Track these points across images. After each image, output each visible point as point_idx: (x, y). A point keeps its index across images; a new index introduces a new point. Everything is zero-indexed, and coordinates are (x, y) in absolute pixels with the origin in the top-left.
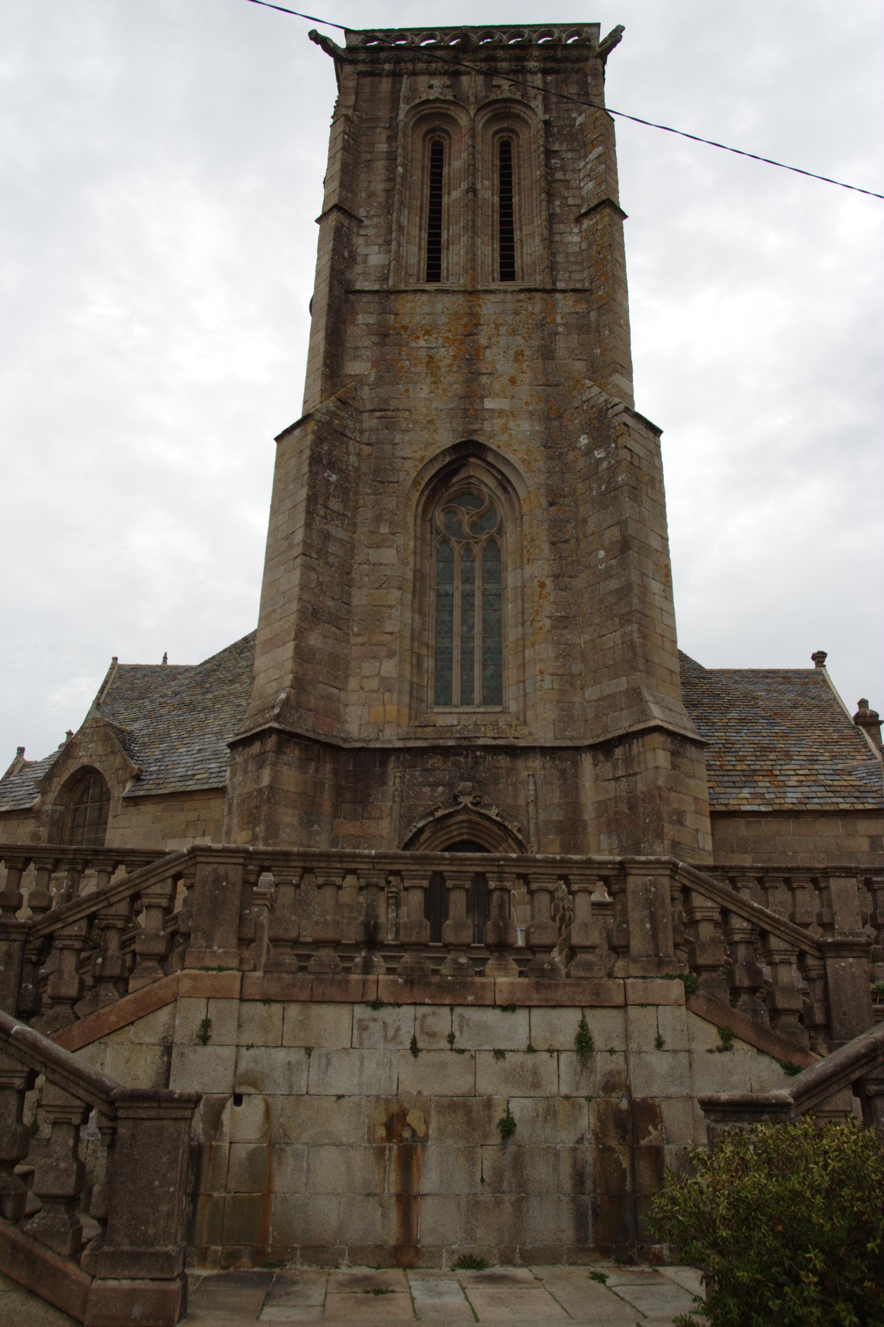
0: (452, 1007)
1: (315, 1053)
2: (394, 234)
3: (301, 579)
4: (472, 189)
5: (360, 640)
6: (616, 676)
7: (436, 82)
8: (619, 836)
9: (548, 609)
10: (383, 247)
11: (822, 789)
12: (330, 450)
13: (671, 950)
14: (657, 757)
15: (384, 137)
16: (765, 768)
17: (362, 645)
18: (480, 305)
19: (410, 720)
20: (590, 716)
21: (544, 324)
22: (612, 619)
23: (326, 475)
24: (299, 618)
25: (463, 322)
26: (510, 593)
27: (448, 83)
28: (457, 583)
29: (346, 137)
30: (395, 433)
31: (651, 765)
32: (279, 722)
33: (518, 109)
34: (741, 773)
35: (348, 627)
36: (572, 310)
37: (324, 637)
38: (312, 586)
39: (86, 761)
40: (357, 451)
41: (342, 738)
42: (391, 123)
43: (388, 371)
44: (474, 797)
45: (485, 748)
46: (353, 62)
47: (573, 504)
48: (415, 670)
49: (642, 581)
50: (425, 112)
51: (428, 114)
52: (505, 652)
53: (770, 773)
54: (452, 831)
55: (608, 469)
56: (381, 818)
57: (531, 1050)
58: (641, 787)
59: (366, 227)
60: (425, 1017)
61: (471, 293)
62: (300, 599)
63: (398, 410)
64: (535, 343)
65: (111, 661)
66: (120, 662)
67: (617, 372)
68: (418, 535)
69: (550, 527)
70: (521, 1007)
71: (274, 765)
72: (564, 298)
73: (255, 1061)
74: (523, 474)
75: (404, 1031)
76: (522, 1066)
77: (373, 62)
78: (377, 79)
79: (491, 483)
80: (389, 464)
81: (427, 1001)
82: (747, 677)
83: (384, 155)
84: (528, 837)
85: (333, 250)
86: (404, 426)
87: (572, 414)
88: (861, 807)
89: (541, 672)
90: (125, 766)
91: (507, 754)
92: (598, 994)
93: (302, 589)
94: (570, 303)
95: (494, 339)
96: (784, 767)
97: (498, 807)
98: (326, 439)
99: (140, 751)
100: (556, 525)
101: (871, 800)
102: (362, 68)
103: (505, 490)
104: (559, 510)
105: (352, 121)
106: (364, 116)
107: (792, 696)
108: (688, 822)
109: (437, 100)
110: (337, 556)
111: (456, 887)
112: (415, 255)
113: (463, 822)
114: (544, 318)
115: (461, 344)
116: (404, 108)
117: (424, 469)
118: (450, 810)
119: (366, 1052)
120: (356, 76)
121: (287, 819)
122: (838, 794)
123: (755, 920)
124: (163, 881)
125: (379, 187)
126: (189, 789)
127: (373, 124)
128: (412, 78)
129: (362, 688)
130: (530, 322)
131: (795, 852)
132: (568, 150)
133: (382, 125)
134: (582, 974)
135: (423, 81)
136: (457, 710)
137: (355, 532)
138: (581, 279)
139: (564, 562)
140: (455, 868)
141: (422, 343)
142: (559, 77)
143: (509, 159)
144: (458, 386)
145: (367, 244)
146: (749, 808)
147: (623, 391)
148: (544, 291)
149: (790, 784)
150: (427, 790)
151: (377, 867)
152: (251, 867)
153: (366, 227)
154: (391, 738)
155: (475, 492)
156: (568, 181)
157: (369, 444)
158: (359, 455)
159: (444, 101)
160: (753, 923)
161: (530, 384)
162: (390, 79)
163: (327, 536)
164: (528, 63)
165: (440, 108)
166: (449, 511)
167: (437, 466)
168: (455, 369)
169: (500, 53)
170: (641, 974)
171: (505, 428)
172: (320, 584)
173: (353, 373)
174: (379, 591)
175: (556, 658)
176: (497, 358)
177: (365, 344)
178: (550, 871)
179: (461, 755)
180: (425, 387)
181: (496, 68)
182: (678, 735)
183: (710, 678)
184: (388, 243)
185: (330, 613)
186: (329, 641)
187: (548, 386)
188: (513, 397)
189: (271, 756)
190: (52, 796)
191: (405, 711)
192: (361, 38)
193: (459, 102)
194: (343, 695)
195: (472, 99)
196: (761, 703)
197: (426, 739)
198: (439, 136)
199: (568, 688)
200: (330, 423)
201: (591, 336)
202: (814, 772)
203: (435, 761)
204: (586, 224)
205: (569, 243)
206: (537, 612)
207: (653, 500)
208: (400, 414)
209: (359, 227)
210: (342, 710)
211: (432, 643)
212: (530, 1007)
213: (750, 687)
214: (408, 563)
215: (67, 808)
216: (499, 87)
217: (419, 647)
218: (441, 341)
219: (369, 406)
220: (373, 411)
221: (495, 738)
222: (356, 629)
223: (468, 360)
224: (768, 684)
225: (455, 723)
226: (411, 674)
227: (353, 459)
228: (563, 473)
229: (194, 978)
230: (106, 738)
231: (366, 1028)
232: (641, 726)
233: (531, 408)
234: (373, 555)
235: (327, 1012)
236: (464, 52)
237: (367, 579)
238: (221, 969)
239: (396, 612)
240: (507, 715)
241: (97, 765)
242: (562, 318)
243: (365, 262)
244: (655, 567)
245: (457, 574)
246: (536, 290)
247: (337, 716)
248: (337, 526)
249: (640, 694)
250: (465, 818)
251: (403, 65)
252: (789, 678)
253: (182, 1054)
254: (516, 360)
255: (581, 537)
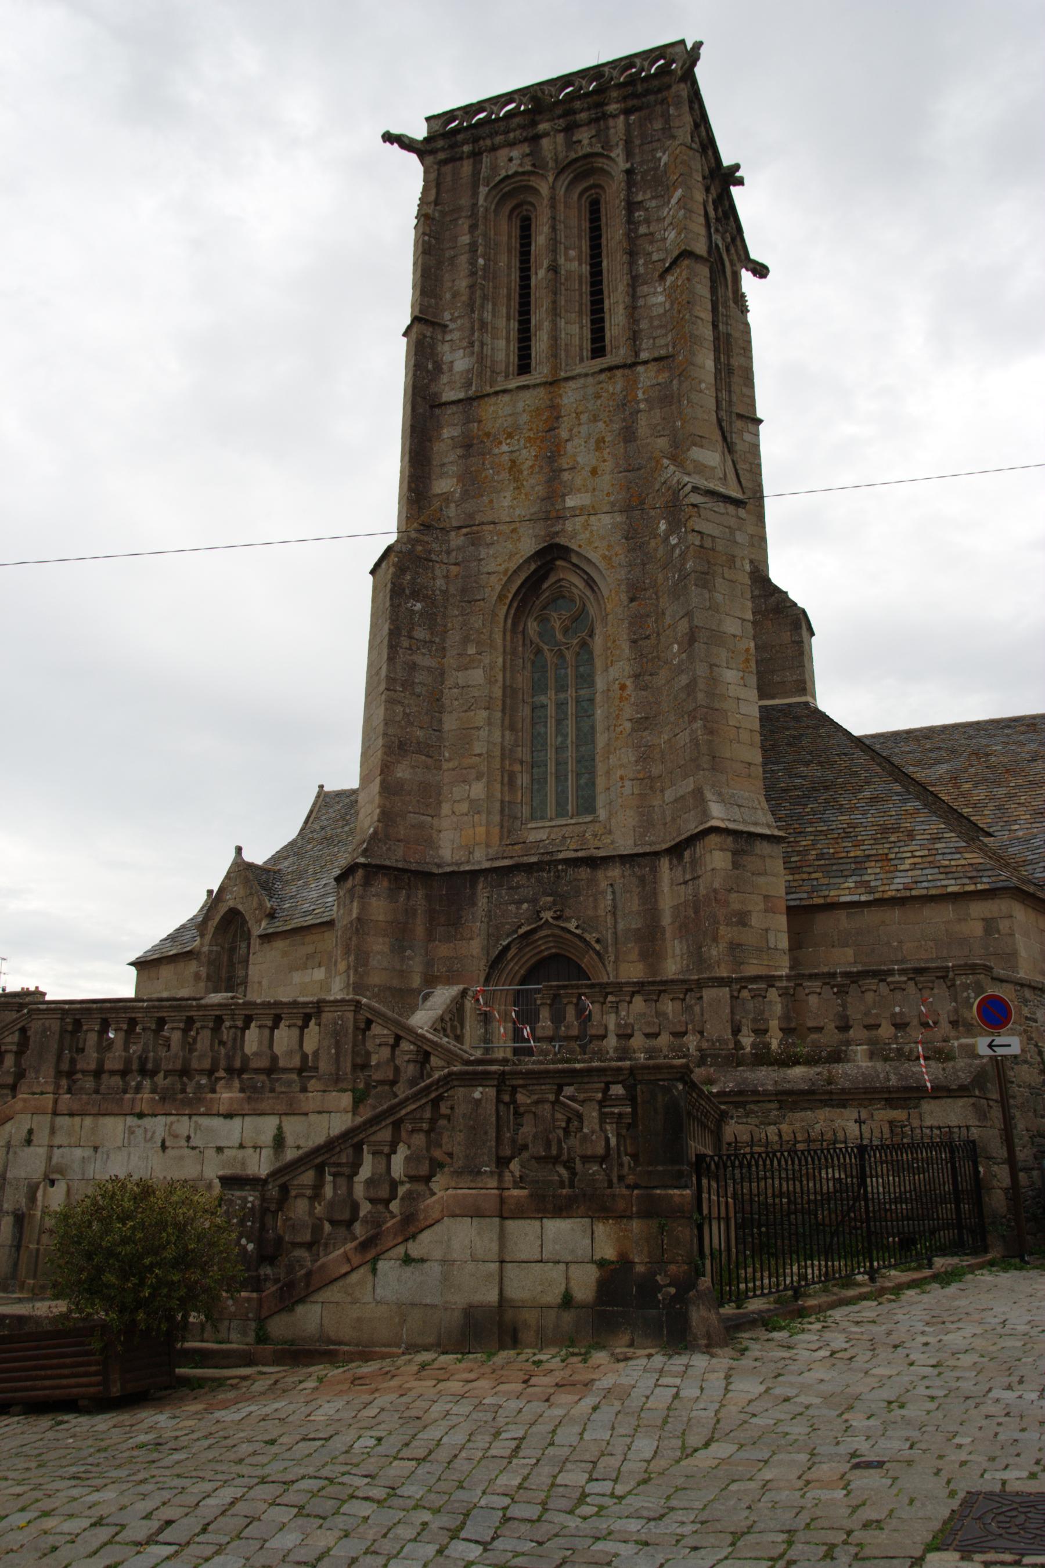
0: (190, 1116)
1: (100, 1150)
2: (476, 334)
3: (385, 715)
4: (577, 249)
5: (451, 765)
6: (685, 776)
7: (515, 153)
8: (687, 940)
9: (628, 711)
10: (468, 350)
11: (936, 870)
12: (413, 579)
13: (349, 1070)
14: (716, 859)
15: (466, 227)
16: (881, 852)
17: (453, 770)
18: (560, 396)
19: (501, 840)
20: (668, 819)
21: (625, 405)
22: (683, 716)
23: (410, 605)
24: (385, 753)
25: (544, 417)
26: (599, 698)
27: (527, 151)
28: (551, 693)
29: (426, 238)
30: (481, 549)
31: (709, 868)
32: (366, 857)
33: (600, 162)
34: (852, 860)
35: (440, 754)
36: (654, 382)
37: (413, 767)
38: (398, 719)
39: (231, 904)
40: (445, 573)
41: (436, 864)
42: (473, 210)
43: (473, 484)
44: (555, 912)
45: (566, 861)
46: (433, 152)
47: (654, 596)
48: (506, 788)
49: (711, 672)
50: (507, 189)
51: (509, 191)
52: (598, 758)
53: (884, 857)
54: (540, 946)
55: (680, 555)
56: (472, 939)
57: (241, 1146)
58: (703, 891)
59: (451, 331)
60: (172, 1123)
61: (551, 384)
62: (385, 734)
63: (483, 524)
64: (616, 426)
65: (317, 789)
66: (326, 789)
67: (695, 445)
68: (508, 649)
69: (631, 624)
70: (236, 1115)
71: (362, 897)
72: (646, 371)
73: (62, 1157)
74: (604, 572)
75: (157, 1134)
76: (235, 1158)
77: (452, 147)
78: (458, 163)
79: (581, 584)
80: (475, 582)
81: (174, 1112)
82: (986, 730)
83: (467, 247)
84: (606, 948)
85: (415, 366)
86: (488, 540)
87: (654, 498)
88: (972, 888)
89: (622, 778)
90: (261, 905)
91: (588, 865)
92: (291, 1105)
93: (386, 724)
94: (652, 374)
95: (575, 430)
96: (902, 850)
97: (578, 919)
98: (408, 568)
99: (282, 889)
100: (637, 621)
101: (985, 880)
102: (441, 156)
103: (593, 590)
104: (640, 605)
105: (433, 219)
106: (447, 209)
107: (1033, 746)
108: (754, 922)
109: (516, 174)
110: (425, 685)
111: (542, 1004)
112: (502, 349)
113: (547, 936)
114: (625, 397)
115: (542, 441)
116: (483, 190)
117: (510, 580)
118: (533, 926)
119: (132, 1149)
120: (436, 167)
121: (377, 948)
122: (950, 876)
123: (419, 1043)
124: (13, 1033)
125: (463, 284)
126: (306, 924)
127: (455, 216)
128: (492, 154)
129: (453, 812)
130: (611, 403)
131: (900, 942)
132: (653, 198)
133: (463, 214)
134: (283, 1089)
135: (503, 154)
136: (553, 823)
137: (444, 657)
138: (663, 344)
139: (645, 660)
140: (201, 1013)
141: (505, 448)
142: (642, 113)
143: (599, 219)
144: (540, 487)
145: (453, 351)
146: (848, 899)
147: (703, 465)
148: (624, 366)
149: (902, 868)
150: (512, 908)
151: (149, 1015)
152: (68, 1020)
153: (451, 331)
154: (480, 860)
155: (567, 594)
156: (652, 234)
157: (455, 564)
158: (446, 577)
159: (523, 173)
160: (419, 1046)
161: (612, 472)
162: (471, 160)
163: (413, 667)
164: (607, 108)
165: (521, 181)
166: (543, 620)
167: (523, 576)
168: (537, 469)
169: (577, 104)
170: (323, 1088)
171: (586, 526)
172: (406, 715)
173: (440, 492)
174: (468, 714)
175: (636, 761)
176: (578, 450)
177: (451, 459)
178: (268, 1011)
179: (543, 870)
180: (508, 494)
181: (575, 121)
182: (742, 832)
183: (853, 754)
184: (472, 344)
185: (419, 743)
186: (419, 770)
187: (629, 471)
188: (594, 489)
189: (359, 890)
190: (208, 938)
191: (496, 830)
192: (440, 122)
193: (538, 167)
194: (435, 821)
195: (551, 164)
196: (994, 759)
197: (512, 857)
198: (527, 210)
199: (649, 791)
200: (411, 552)
201: (673, 407)
202: (934, 852)
203: (520, 879)
204: (670, 279)
205: (653, 305)
206: (618, 716)
207: (731, 581)
208: (485, 527)
209: (444, 333)
210: (435, 836)
211: (527, 758)
212: (243, 1115)
213: (984, 741)
214: (496, 681)
215: (223, 948)
216: (580, 142)
217: (510, 765)
218: (522, 442)
219: (455, 524)
220: (460, 528)
221: (576, 850)
222: (447, 755)
223: (549, 457)
224: (1008, 735)
225: (545, 838)
226: (502, 793)
227: (440, 583)
228: (644, 565)
229: (25, 1100)
230: (247, 881)
231: (133, 1133)
232: (701, 828)
233: (612, 499)
234: (461, 677)
235: (108, 1122)
236: (540, 113)
237: (456, 703)
238: (42, 1093)
239: (483, 733)
240: (598, 824)
241: (240, 907)
242: (644, 393)
243: (451, 369)
244: (730, 654)
245: (551, 683)
246: (617, 367)
247: (430, 843)
248: (424, 654)
249: (702, 794)
250: (549, 932)
251: (481, 142)
252: (1034, 725)
253: (15, 1153)
254: (598, 448)
255: (661, 631)
